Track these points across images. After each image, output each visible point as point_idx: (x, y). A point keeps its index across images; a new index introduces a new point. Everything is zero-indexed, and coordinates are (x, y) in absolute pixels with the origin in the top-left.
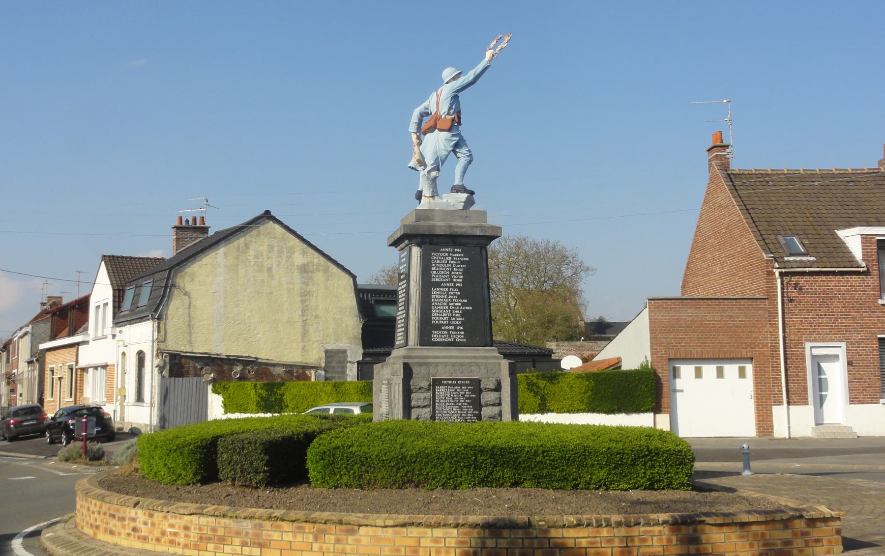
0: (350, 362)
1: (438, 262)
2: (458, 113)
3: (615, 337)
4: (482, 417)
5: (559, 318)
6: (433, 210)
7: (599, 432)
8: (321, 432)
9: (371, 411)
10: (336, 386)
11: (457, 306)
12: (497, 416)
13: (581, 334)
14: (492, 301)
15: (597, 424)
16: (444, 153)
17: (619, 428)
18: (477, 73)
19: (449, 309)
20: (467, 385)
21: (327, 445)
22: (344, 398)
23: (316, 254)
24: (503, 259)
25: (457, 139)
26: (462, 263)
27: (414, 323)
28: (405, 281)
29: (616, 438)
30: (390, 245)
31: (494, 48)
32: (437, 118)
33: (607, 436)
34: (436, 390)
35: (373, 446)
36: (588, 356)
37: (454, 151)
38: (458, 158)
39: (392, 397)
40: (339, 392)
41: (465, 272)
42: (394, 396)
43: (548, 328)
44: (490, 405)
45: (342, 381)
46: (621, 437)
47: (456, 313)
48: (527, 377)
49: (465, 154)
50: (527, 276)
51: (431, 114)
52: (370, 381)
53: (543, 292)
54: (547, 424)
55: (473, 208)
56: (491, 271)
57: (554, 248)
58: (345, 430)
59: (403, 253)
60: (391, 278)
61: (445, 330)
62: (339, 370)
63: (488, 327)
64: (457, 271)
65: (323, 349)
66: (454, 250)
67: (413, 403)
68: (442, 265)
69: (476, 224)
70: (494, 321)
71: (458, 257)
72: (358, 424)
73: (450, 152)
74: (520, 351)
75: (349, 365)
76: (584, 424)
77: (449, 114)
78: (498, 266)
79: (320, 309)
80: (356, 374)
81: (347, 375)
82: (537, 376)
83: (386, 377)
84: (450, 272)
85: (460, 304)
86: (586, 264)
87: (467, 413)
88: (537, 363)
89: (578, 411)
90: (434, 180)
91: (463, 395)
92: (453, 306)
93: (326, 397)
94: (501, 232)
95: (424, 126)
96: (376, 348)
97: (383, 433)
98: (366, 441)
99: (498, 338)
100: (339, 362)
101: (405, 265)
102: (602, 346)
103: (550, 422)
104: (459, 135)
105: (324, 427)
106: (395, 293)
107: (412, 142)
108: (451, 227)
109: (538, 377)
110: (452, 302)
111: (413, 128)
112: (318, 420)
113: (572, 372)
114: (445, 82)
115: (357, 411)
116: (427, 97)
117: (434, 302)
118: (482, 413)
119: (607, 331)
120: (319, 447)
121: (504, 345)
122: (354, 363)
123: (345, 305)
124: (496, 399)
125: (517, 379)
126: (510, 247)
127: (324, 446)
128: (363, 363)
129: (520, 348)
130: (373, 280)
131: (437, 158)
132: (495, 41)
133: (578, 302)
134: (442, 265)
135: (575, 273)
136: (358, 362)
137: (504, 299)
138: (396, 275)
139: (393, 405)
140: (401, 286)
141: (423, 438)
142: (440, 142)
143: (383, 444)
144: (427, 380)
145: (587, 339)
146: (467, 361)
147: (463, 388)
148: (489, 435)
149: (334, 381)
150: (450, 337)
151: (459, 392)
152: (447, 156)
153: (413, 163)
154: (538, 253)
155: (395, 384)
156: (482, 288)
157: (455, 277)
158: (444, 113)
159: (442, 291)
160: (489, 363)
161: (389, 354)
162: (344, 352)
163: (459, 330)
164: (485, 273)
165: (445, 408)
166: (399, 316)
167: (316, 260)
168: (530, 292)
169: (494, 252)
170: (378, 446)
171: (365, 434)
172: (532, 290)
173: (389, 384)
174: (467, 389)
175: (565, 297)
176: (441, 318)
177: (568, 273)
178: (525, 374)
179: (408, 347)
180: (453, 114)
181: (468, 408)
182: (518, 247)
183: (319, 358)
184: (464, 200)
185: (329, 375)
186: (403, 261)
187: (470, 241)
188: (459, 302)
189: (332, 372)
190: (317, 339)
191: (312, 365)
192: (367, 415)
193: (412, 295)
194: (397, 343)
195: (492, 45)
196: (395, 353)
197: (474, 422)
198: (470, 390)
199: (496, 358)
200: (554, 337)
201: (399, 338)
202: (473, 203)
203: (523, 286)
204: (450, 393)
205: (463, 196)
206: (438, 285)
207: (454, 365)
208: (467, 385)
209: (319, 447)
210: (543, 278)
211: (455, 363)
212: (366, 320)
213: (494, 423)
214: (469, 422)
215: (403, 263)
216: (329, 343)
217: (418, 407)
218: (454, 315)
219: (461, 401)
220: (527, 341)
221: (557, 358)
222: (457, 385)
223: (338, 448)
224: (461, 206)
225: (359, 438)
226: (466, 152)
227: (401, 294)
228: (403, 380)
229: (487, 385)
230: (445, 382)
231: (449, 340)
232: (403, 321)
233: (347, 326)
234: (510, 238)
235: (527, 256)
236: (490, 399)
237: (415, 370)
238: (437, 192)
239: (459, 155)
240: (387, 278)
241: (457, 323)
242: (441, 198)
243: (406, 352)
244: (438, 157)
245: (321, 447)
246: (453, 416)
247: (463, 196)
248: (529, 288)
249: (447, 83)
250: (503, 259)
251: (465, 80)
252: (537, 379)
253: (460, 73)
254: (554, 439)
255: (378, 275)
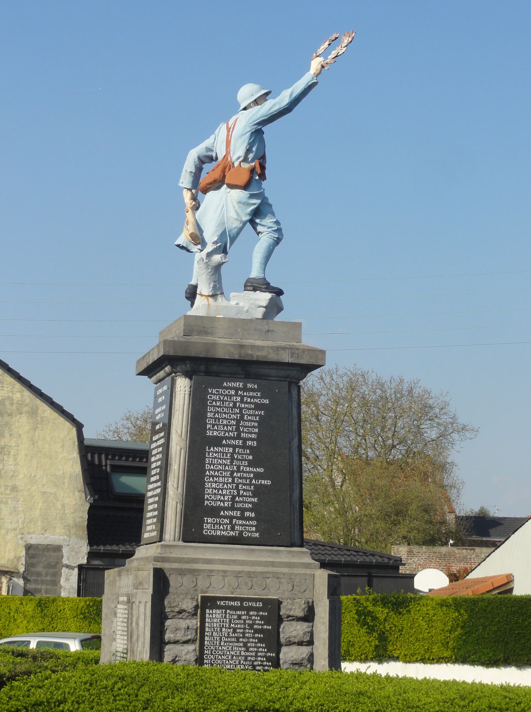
0: (67, 566)
1: (218, 404)
2: (262, 159)
3: (504, 542)
4: (281, 662)
5: (414, 506)
6: (212, 319)
7: (471, 693)
8: (12, 678)
9: (98, 648)
10: (41, 605)
11: (246, 478)
12: (305, 662)
13: (449, 535)
14: (305, 475)
15: (469, 681)
16: (234, 226)
17: (506, 689)
18: (294, 95)
19: (233, 482)
20: (257, 609)
21: (21, 698)
22: (55, 625)
23: (18, 385)
24: (326, 406)
25: (258, 202)
26: (258, 407)
27: (174, 503)
28: (162, 434)
29: (499, 704)
30: (141, 374)
31: (325, 54)
32: (227, 166)
33: (486, 701)
34: (207, 615)
35: (98, 704)
36: (459, 571)
37: (252, 222)
38: (258, 233)
39: (134, 624)
40: (45, 615)
41: (262, 423)
42: (137, 624)
43: (395, 523)
44: (294, 643)
45: (52, 596)
46: (507, 703)
47: (244, 490)
48: (358, 601)
49: (269, 228)
50: (364, 437)
51: (217, 158)
52: (99, 599)
53: (389, 463)
54: (388, 677)
55: (279, 318)
56: (306, 425)
57: (410, 391)
58: (53, 676)
59: (162, 387)
60: (141, 430)
61: (226, 517)
62: (48, 578)
63: (297, 514)
64: (250, 421)
65: (22, 543)
66: (245, 386)
67: (168, 636)
68: (225, 410)
69: (283, 344)
70: (307, 508)
71: (251, 397)
72: (75, 666)
73: (245, 224)
74: (349, 559)
75: (64, 570)
76: (447, 679)
77: (245, 160)
78: (317, 417)
79: (21, 476)
80: (75, 586)
81: (61, 587)
82: (374, 599)
83: (124, 591)
84: (238, 422)
85: (252, 475)
86: (462, 420)
87: (256, 656)
88: (375, 580)
89: (439, 660)
90: (217, 268)
91: (251, 626)
92: (240, 478)
93: (25, 622)
94: (324, 359)
95: (205, 179)
96: (111, 545)
97: (116, 683)
98: (87, 694)
99: (311, 535)
100: (49, 566)
101: (164, 407)
102: (483, 556)
103: (392, 674)
104: (261, 196)
105: (19, 669)
106: (145, 455)
107: (184, 205)
108: (241, 346)
109: (375, 602)
110: (238, 471)
111: (185, 181)
112: (9, 658)
113: (431, 596)
114: (242, 107)
115: (74, 646)
116: (210, 131)
117: (209, 470)
118: (281, 656)
119: (492, 531)
120: (8, 701)
121: (323, 548)
122: (72, 568)
123: (61, 472)
124: (305, 634)
125: (341, 602)
126: (337, 387)
127: (18, 700)
128: (87, 569)
129: (349, 553)
130: (111, 433)
131: (224, 232)
132: (327, 43)
133: (446, 482)
134: (225, 410)
135: (442, 435)
136: (81, 567)
137: (326, 473)
138: (149, 426)
139: (135, 637)
140: (156, 441)
141: (182, 693)
142: (230, 205)
143: (115, 700)
144: (192, 599)
145: (460, 543)
146: (259, 569)
147: (251, 613)
148: (291, 692)
149: (38, 596)
150: (233, 529)
151: (245, 620)
152: (241, 229)
153: (183, 239)
154: (384, 398)
155: (140, 602)
156: (290, 449)
157: (245, 430)
158: (239, 158)
159: (223, 453)
160: (296, 575)
161: (131, 554)
162: (58, 549)
163: (249, 519)
164: (295, 427)
165: (220, 645)
166: (150, 490)
167: (18, 395)
168: (368, 462)
169: (311, 395)
170: (108, 703)
171: (85, 683)
172: (372, 460)
173: (130, 603)
174: (257, 616)
175: (425, 474)
176: (219, 497)
177: (432, 434)
178: (354, 596)
179: (162, 543)
180: (252, 161)
181: (258, 648)
182: (352, 387)
183: (15, 557)
184: (264, 303)
185: (30, 586)
186: (160, 400)
187: (273, 372)
188: (251, 472)
189: (36, 581)
190: (14, 526)
191: (4, 569)
192: (90, 653)
193: (173, 456)
194: (146, 535)
195: (321, 50)
196: (141, 552)
197: (268, 670)
198: (262, 618)
199: (306, 566)
200: (405, 538)
201: (149, 528)
202: (280, 309)
203: (356, 452)
204: (230, 621)
205: (264, 297)
206: (217, 441)
207: (237, 575)
208: (257, 609)
209: (8, 701)
210: (390, 441)
211: (239, 572)
212: (97, 497)
213: (300, 673)
214: (259, 670)
215: (162, 404)
216: (33, 533)
217: (176, 642)
218: (241, 492)
219: (247, 635)
220: (360, 542)
221: (408, 572)
222: (241, 608)
223: (40, 705)
224: (259, 313)
225: (75, 689)
226: (271, 225)
227: (155, 455)
228: (153, 596)
229: (291, 610)
230: (222, 603)
231: (232, 533)
232: (156, 499)
233: (63, 506)
234: (340, 373)
235: (365, 403)
236: (294, 633)
237: (174, 581)
238: (221, 288)
239: (259, 228)
240: (133, 430)
241: (246, 506)
242: (228, 299)
243: (159, 550)
244: (225, 230)
245: (13, 702)
246: (232, 659)
247: (264, 297)
248: (367, 456)
249: (245, 109)
250: (326, 406)
251: (275, 105)
252: (374, 605)
253: (267, 94)
254: (397, 702)
255: (119, 425)
